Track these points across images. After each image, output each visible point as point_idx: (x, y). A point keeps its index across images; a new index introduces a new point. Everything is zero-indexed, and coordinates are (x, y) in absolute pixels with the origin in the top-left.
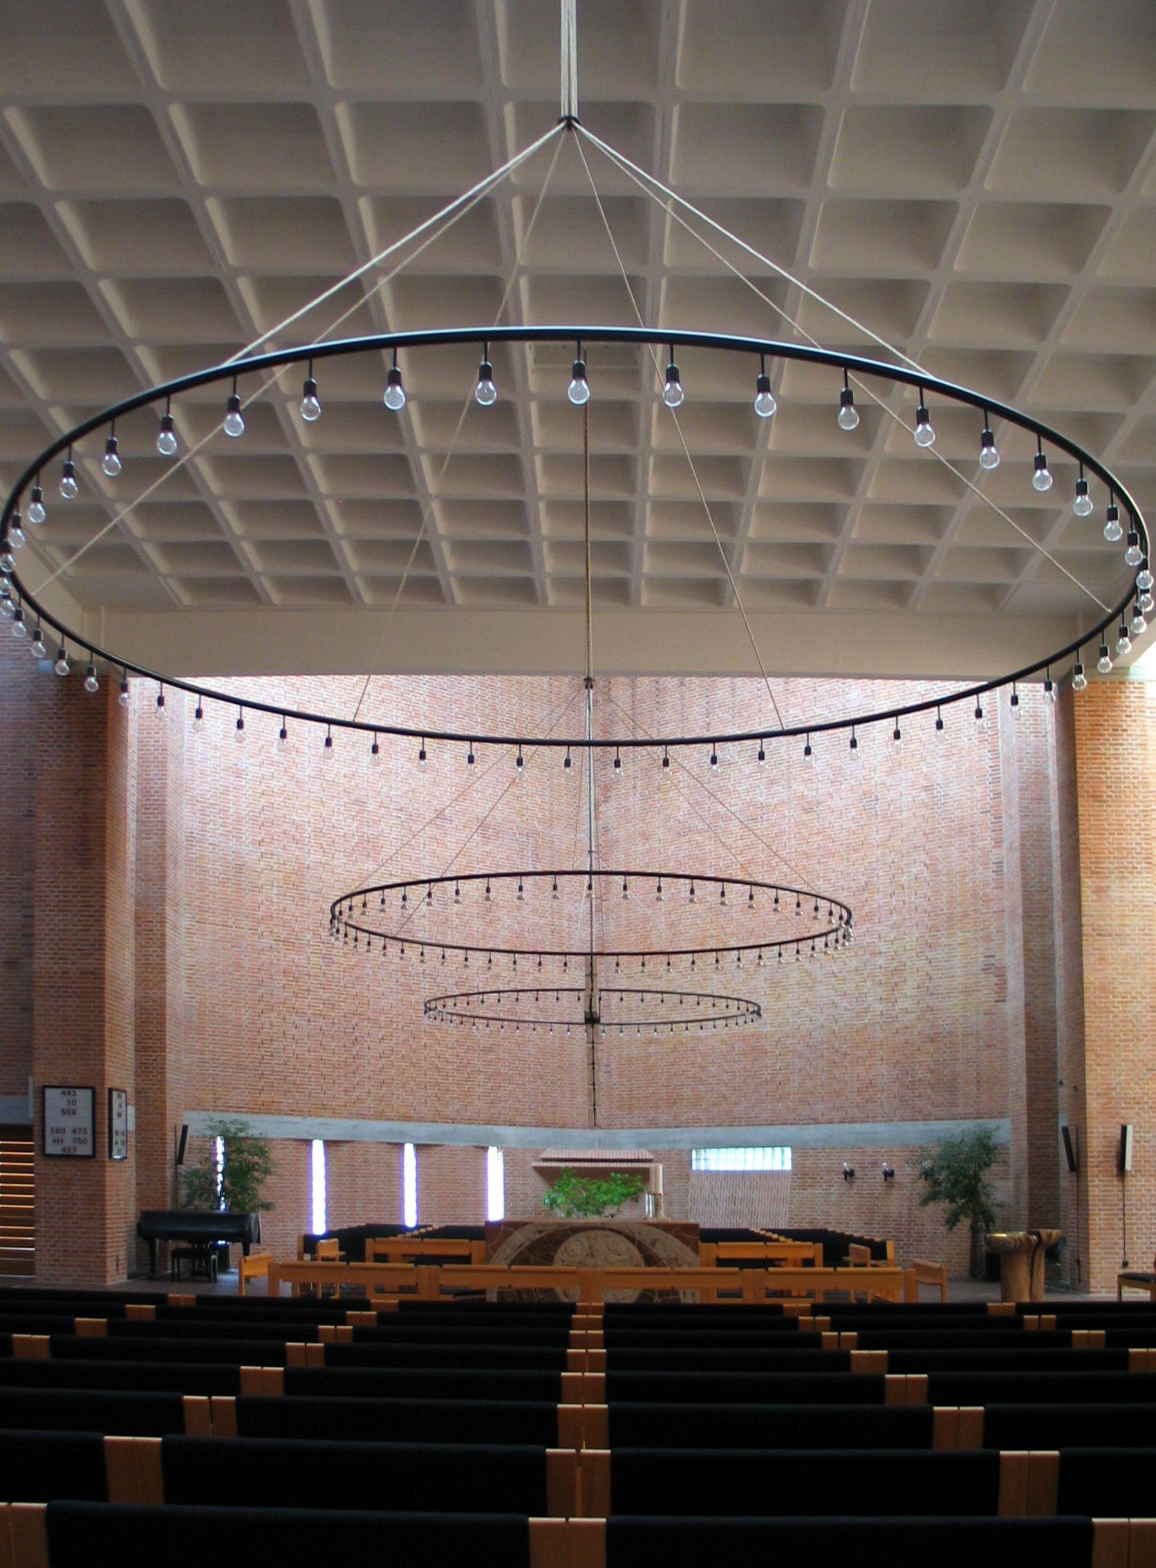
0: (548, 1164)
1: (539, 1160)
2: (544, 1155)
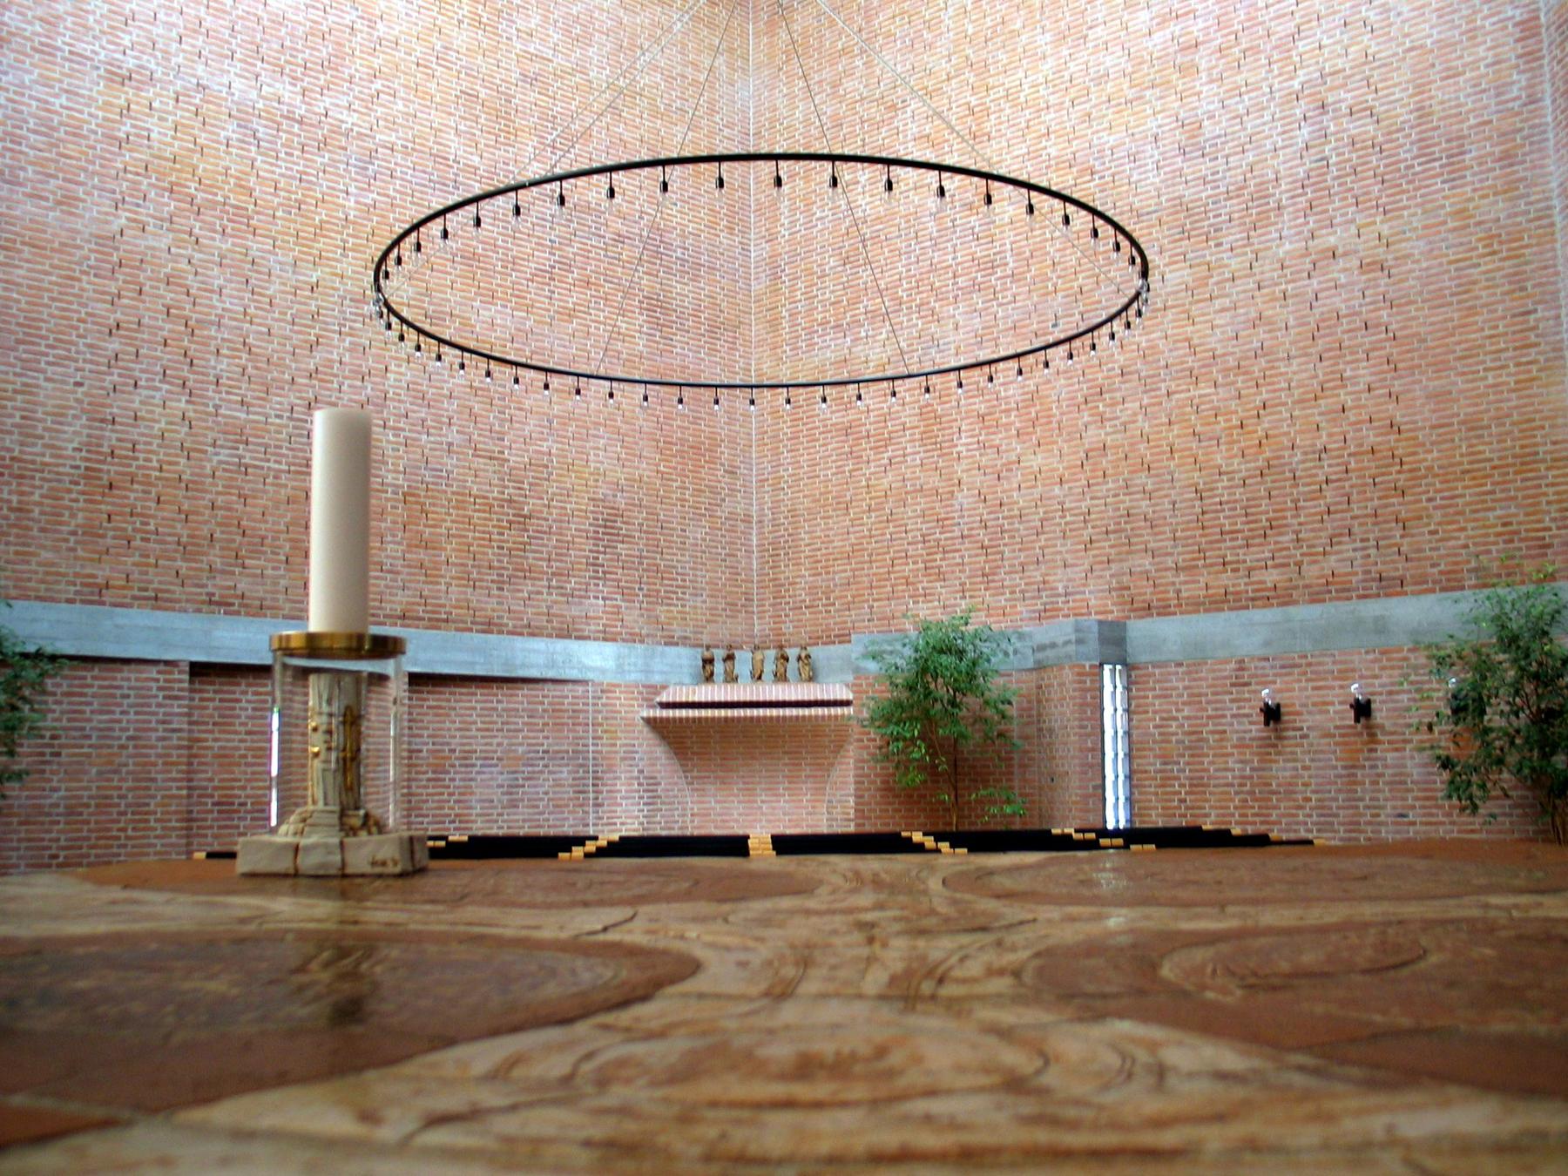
0: (670, 713)
1: (653, 707)
2: (665, 697)
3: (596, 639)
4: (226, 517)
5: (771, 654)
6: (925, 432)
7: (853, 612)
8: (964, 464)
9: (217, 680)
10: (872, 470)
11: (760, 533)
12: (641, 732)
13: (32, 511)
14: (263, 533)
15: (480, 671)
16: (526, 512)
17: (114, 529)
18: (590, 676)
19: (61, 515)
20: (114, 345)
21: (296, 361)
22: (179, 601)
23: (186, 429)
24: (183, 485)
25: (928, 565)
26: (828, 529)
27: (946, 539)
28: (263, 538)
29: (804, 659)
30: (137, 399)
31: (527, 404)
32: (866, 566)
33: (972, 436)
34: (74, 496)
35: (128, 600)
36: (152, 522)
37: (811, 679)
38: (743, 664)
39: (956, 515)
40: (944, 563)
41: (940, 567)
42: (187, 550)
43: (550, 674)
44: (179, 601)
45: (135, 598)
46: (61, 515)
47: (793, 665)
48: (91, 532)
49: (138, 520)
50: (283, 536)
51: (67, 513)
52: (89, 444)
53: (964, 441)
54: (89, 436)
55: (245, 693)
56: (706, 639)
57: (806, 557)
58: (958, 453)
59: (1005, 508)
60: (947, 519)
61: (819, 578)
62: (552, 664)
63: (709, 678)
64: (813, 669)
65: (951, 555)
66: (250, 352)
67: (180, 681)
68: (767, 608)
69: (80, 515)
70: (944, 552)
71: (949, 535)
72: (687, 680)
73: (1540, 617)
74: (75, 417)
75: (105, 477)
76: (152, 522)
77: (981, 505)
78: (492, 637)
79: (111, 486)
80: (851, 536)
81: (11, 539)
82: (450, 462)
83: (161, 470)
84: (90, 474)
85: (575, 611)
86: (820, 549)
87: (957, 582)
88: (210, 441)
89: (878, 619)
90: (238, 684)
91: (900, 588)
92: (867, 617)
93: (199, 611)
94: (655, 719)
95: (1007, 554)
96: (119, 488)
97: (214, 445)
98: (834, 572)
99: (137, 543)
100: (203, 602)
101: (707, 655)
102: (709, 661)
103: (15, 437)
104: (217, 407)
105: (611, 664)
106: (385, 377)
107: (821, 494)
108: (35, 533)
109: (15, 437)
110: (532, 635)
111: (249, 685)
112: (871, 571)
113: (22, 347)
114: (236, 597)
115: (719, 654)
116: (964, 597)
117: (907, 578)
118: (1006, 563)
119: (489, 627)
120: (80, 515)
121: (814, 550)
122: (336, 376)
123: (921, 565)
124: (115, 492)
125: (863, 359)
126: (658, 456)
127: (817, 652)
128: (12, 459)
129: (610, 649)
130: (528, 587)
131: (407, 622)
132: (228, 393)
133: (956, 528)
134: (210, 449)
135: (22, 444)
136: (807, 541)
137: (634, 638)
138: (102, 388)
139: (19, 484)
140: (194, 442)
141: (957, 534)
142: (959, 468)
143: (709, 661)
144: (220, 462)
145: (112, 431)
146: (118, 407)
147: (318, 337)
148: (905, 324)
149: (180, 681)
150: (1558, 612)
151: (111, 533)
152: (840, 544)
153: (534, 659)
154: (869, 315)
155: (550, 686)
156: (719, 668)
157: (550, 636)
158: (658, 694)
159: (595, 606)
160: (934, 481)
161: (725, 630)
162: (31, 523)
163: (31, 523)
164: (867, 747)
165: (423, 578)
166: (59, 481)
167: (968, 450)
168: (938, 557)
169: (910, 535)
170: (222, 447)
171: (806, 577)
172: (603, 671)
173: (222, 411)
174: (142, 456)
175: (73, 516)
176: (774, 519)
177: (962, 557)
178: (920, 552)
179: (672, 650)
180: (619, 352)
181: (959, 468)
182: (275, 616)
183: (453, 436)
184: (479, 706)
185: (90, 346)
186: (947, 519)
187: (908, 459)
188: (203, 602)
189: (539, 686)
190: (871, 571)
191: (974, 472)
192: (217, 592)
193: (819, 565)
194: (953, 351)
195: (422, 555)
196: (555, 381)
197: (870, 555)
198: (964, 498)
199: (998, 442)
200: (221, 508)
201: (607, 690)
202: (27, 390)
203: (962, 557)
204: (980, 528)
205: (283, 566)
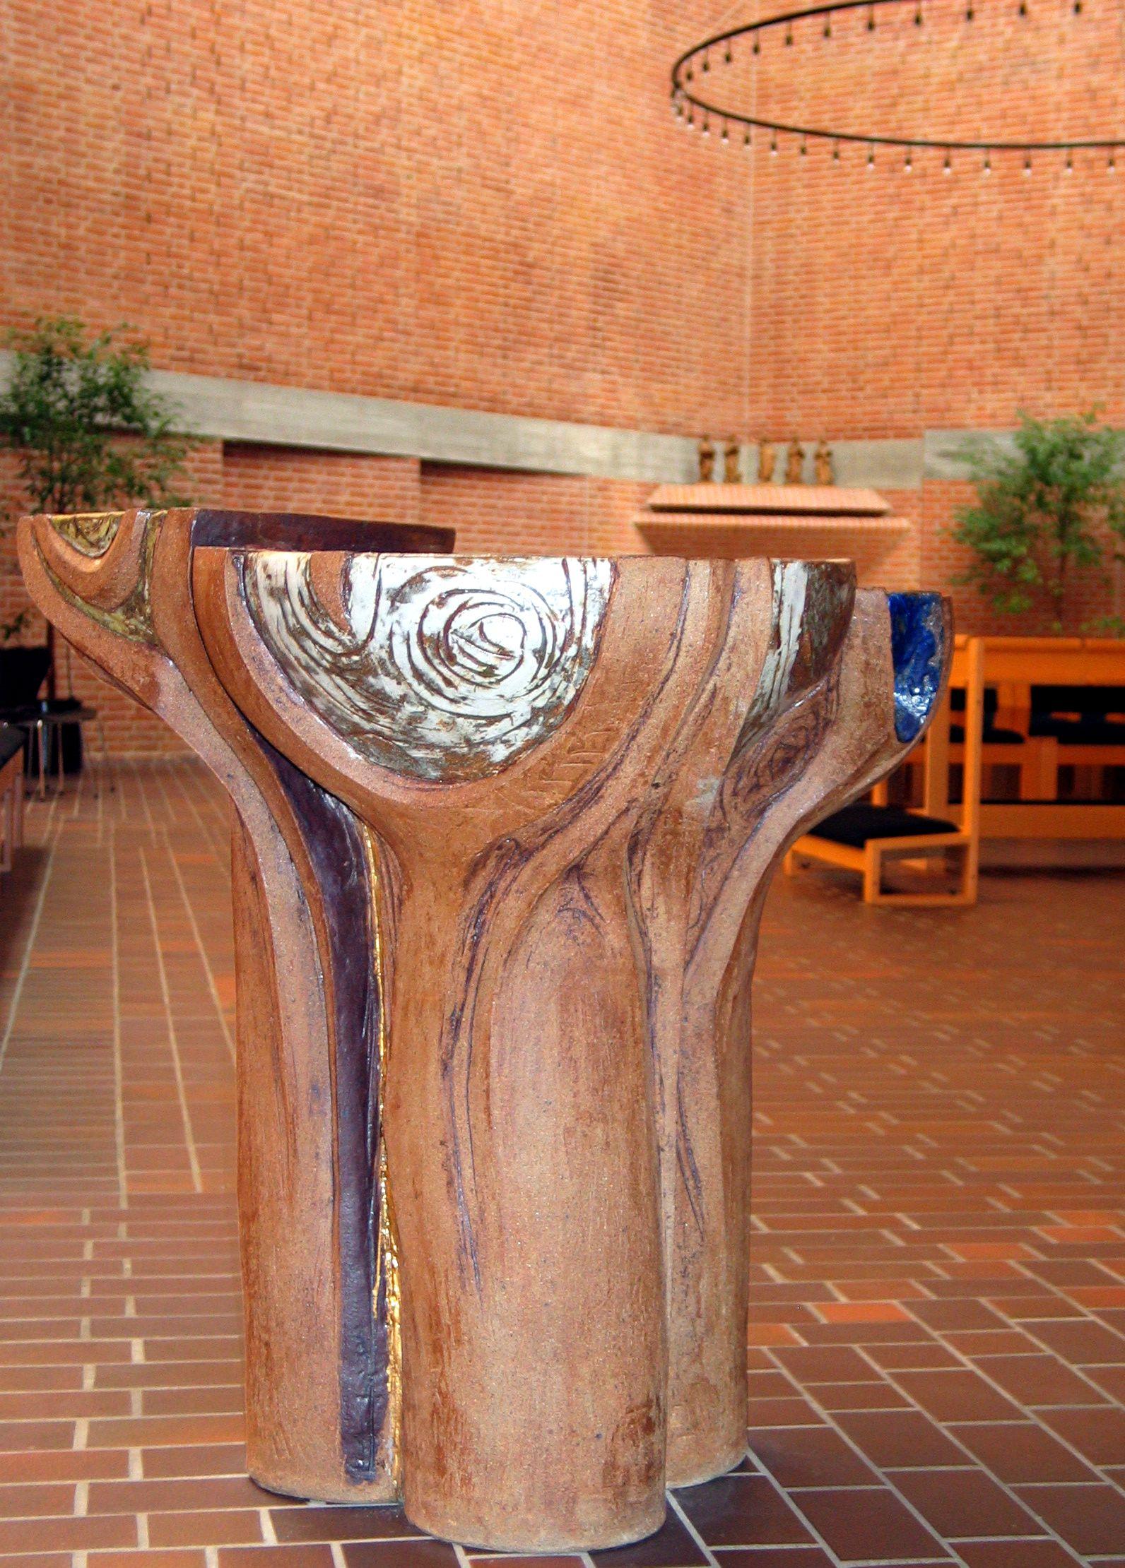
2: (659, 499)
3: (594, 423)
4: (254, 260)
5: (782, 450)
6: (1006, 176)
7: (891, 400)
8: (1061, 221)
9: (243, 461)
10: (928, 220)
11: (756, 292)
13: (77, 249)
14: (287, 281)
15: (485, 459)
16: (530, 259)
17: (154, 273)
18: (588, 469)
19: (103, 254)
20: (146, 37)
21: (315, 59)
22: (211, 364)
23: (214, 148)
24: (213, 218)
25: (1003, 345)
26: (859, 293)
27: (1030, 315)
28: (287, 287)
29: (824, 458)
30: (170, 107)
31: (534, 118)
32: (912, 342)
33: (1075, 186)
34: (115, 230)
35: (166, 361)
36: (187, 264)
37: (830, 483)
38: (747, 462)
39: (1045, 285)
40: (1024, 344)
41: (1017, 349)
42: (220, 300)
43: (550, 465)
44: (211, 364)
45: (174, 359)
46: (103, 254)
47: (809, 464)
48: (131, 276)
49: (174, 261)
50: (306, 285)
51: (110, 251)
52: (127, 165)
53: (1062, 191)
54: (128, 154)
55: (266, 478)
56: (698, 428)
57: (825, 327)
58: (1054, 207)
59: (1113, 280)
60: (1031, 289)
61: (842, 355)
62: (551, 454)
63: (706, 477)
64: (833, 470)
65: (1035, 335)
66: (273, 49)
67: (214, 462)
68: (763, 389)
69: (123, 254)
70: (1026, 331)
71: (1032, 310)
72: (678, 478)
73: (576, 411)
74: (115, 130)
75: (144, 206)
76: (187, 264)
77: (1081, 275)
78: (497, 418)
79: (149, 219)
80: (893, 303)
81: (62, 283)
82: (460, 193)
83: (194, 199)
84: (130, 203)
85: (574, 387)
86: (844, 318)
87: (1040, 369)
88: (236, 162)
89: (928, 411)
90: (258, 467)
91: (961, 372)
92: (910, 407)
93: (229, 376)
95: (1112, 339)
96: (157, 222)
97: (241, 168)
98: (867, 349)
99: (173, 291)
100: (233, 366)
101: (706, 446)
102: (707, 456)
103: (61, 155)
104: (243, 119)
105: (605, 455)
106: (398, 82)
107: (851, 246)
108: (82, 276)
109: (61, 155)
110: (535, 415)
111: (272, 469)
112: (921, 350)
113: (64, 38)
114: (263, 360)
115: (719, 447)
116: (1049, 389)
117: (970, 361)
118: (1112, 349)
119: (495, 405)
120: (123, 254)
121: (837, 319)
122: (352, 79)
123: (991, 346)
124: (154, 226)
125: (922, 72)
126: (657, 189)
127: (840, 449)
128: (61, 183)
129: (607, 435)
130: (531, 355)
131: (420, 395)
132: (254, 101)
133: (1043, 302)
134: (237, 173)
135: (68, 164)
136: (828, 307)
137: (631, 424)
138: (138, 93)
139: (67, 215)
140: (223, 164)
141: (1044, 309)
142: (1052, 227)
143: (707, 456)
144: (248, 191)
145: (149, 148)
146: (154, 118)
147: (336, 27)
148: (986, 31)
149: (214, 462)
150: (127, 369)
151: (150, 278)
152: (877, 312)
153: (539, 447)
154: (935, 13)
155: (548, 481)
156: (719, 466)
157: (550, 418)
159: (593, 380)
160: (1016, 240)
161: (718, 416)
162: (78, 264)
163: (78, 264)
164: (936, 567)
165: (432, 341)
166: (102, 211)
167: (1067, 204)
168: (1017, 336)
169: (978, 307)
170: (249, 171)
171: (823, 352)
172: (599, 463)
173: (249, 125)
174: (176, 180)
175: (115, 255)
176: (778, 275)
177: (1050, 339)
178: (992, 329)
179: (665, 440)
180: (622, 48)
181: (1052, 227)
182: (299, 385)
183: (463, 162)
184: (481, 501)
185: (125, 37)
186: (1031, 289)
187: (981, 208)
188: (233, 366)
189: (536, 480)
190: (921, 350)
191: (1073, 233)
192: (247, 353)
193: (844, 338)
194: (1054, 73)
195: (431, 312)
196: (847, 149)
197: (918, 329)
198: (1056, 265)
199: (1108, 197)
200: (249, 249)
201: (604, 487)
202: (69, 94)
203: (1050, 339)
204: (1076, 303)
205: (306, 322)
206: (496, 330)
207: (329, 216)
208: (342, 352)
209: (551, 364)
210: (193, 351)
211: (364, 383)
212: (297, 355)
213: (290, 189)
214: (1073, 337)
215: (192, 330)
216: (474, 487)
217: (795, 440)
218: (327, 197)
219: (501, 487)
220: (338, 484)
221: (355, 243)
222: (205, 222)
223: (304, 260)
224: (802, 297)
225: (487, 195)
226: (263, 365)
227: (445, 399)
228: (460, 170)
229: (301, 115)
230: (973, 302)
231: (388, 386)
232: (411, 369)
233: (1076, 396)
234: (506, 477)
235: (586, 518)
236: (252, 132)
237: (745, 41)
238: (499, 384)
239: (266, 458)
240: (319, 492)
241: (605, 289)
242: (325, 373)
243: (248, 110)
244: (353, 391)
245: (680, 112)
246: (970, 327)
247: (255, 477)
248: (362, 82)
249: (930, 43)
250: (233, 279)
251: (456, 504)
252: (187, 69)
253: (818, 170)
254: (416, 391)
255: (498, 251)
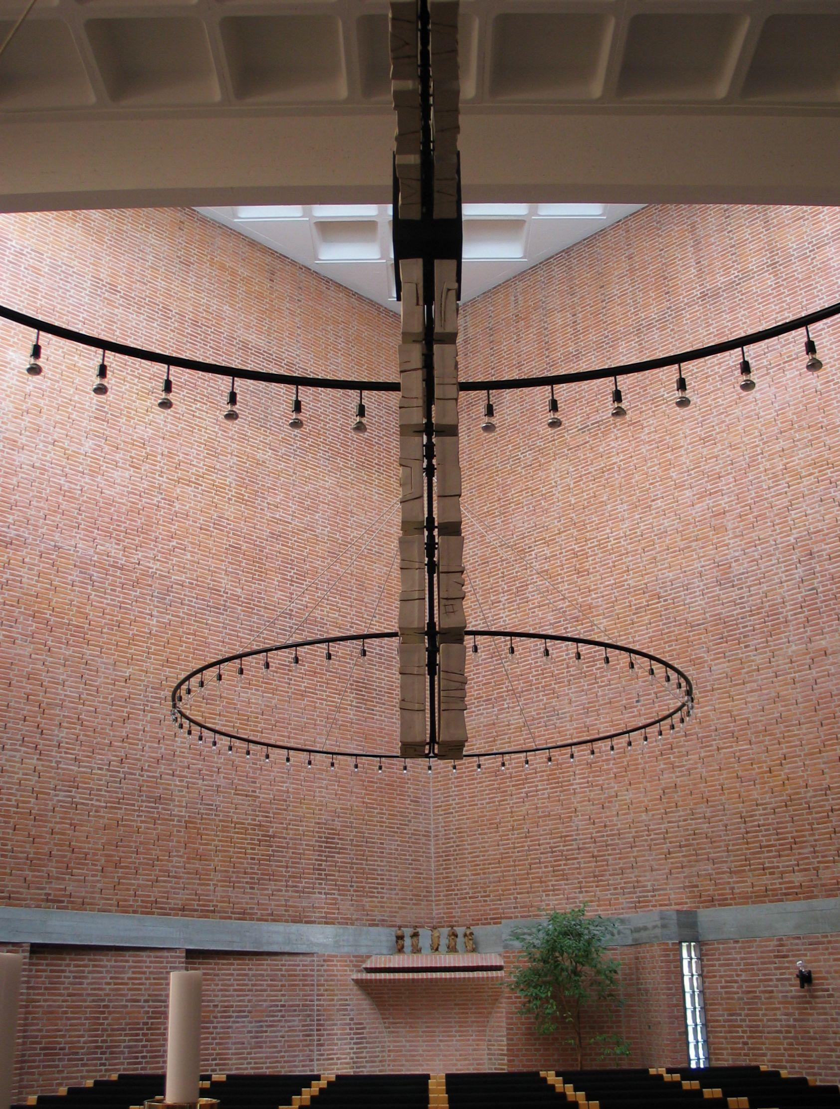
0: (373, 976)
2: (368, 965)
5: (445, 931)
12: (351, 990)
24: (32, 817)
37: (474, 951)
38: (425, 941)
41: (563, 870)
43: (287, 949)
47: (460, 940)
63: (401, 950)
72: (385, 951)
82: (218, 799)
90: (64, 959)
93: (39, 906)
94: (362, 980)
95: (610, 862)
101: (399, 933)
102: (400, 938)
104: (58, 763)
105: (330, 941)
111: (71, 960)
119: (244, 915)
127: (477, 930)
129: (330, 930)
137: (347, 922)
143: (400, 938)
156: (408, 942)
158: (363, 962)
159: (319, 899)
170: (60, 790)
172: (325, 946)
183: (221, 781)
184: (235, 972)
189: (278, 958)
195: (197, 865)
198: (579, 822)
200: (57, 833)
206: (245, 873)
207: (120, 814)
208: (128, 890)
209: (287, 891)
210: (10, 892)
211: (142, 907)
212: (93, 893)
213: (91, 800)
214: (589, 862)
215: (11, 880)
216: (233, 964)
217: (452, 927)
218: (119, 803)
219: (250, 963)
220: (124, 967)
221: (140, 827)
222: (26, 819)
223: (99, 838)
224: (457, 846)
225: (238, 799)
226: (66, 899)
227: (205, 913)
228: (218, 786)
229: (102, 760)
230: (539, 845)
231: (162, 908)
232: (180, 898)
233: (595, 896)
234: (254, 958)
235: (315, 978)
236: (64, 769)
237: (212, 673)
238: (247, 903)
239: (68, 954)
240: (107, 972)
241: (326, 847)
242: (114, 902)
243: (61, 757)
244: (135, 912)
245: (176, 720)
246: (539, 858)
247: (60, 965)
248: (147, 741)
249: (508, 708)
250: (46, 850)
251: (218, 975)
252: (19, 737)
253: (462, 777)
254: (183, 910)
255: (247, 829)
